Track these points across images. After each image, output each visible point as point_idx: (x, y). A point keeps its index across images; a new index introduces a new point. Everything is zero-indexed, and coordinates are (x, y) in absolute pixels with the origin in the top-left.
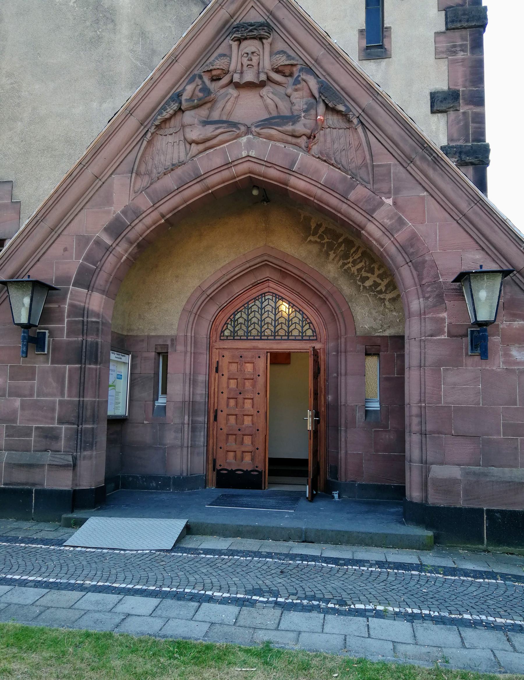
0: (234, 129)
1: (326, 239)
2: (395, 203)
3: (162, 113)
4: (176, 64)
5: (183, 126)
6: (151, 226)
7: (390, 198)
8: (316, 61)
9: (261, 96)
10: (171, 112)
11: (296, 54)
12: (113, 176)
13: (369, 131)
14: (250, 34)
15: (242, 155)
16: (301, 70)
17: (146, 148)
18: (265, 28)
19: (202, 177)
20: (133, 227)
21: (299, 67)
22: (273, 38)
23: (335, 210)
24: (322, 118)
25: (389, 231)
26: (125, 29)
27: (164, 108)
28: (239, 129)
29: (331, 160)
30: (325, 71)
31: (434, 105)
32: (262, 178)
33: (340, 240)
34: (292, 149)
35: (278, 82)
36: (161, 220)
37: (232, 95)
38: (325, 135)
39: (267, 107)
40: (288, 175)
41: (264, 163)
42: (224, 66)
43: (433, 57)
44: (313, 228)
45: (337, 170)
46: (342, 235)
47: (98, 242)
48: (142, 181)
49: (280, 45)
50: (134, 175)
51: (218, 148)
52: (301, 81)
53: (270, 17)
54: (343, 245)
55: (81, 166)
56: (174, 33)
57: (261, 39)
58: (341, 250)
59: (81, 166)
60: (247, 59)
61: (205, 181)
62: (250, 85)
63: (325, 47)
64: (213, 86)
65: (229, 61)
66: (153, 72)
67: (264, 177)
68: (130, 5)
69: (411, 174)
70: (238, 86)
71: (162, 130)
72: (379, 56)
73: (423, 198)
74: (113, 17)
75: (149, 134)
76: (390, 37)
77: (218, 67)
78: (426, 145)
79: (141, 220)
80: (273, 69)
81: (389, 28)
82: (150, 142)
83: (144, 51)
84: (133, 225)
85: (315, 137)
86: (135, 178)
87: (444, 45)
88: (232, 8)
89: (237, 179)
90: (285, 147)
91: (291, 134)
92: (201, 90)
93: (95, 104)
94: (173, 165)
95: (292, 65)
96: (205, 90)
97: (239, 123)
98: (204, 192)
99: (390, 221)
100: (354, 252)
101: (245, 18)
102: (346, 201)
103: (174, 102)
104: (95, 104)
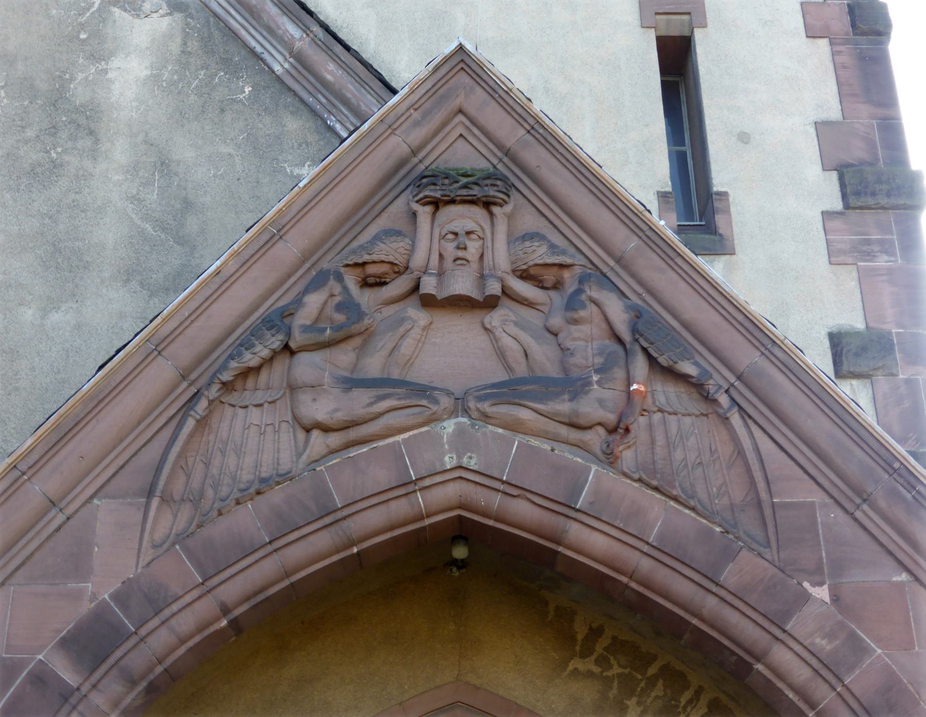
0: (424, 402)
1: (616, 666)
2: (836, 598)
3: (240, 355)
4: (280, 244)
5: (293, 388)
6: (191, 636)
7: (821, 584)
8: (618, 261)
9: (486, 329)
10: (265, 353)
11: (566, 243)
12: (96, 501)
13: (756, 422)
14: (464, 192)
15: (443, 464)
16: (582, 280)
17: (191, 435)
18: (499, 183)
19: (339, 515)
20: (142, 640)
21: (578, 270)
22: (515, 206)
23: (687, 610)
24: (643, 389)
25: (829, 669)
26: (119, 152)
27: (245, 344)
28: (436, 402)
29: (674, 487)
30: (641, 283)
31: (841, 362)
32: (491, 523)
33: (652, 670)
34: (570, 457)
35: (526, 300)
36: (218, 619)
37: (414, 321)
38: (650, 426)
39: (501, 354)
40: (562, 519)
41: (502, 487)
42: (397, 255)
43: (825, 259)
44: (580, 637)
45: (687, 511)
46: (655, 658)
47: (41, 679)
48: (175, 516)
49: (529, 221)
50: (155, 502)
51: (381, 443)
52: (587, 303)
53: (506, 160)
54: (661, 682)
55: (17, 473)
56: (239, 168)
57: (487, 204)
58: (657, 697)
59: (17, 473)
60: (455, 244)
61: (344, 524)
62: (460, 303)
63: (641, 234)
64: (366, 298)
65: (408, 247)
66: (223, 259)
67: (497, 520)
68: (135, 104)
69: (865, 529)
70: (429, 302)
71: (235, 393)
72: (709, 250)
73: (901, 584)
74: (92, 125)
75: (203, 404)
76: (727, 211)
77: (383, 258)
78: (897, 465)
79: (167, 620)
80: (514, 271)
81: (724, 195)
82: (203, 423)
83: (164, 202)
84: (143, 631)
85: (627, 430)
86: (159, 509)
87: (845, 239)
88: (417, 136)
89: (427, 522)
90: (553, 450)
91: (566, 420)
92: (339, 307)
93: (30, 312)
94: (263, 481)
95: (562, 266)
96: (348, 306)
97: (435, 389)
98: (338, 551)
99: (830, 642)
100: (690, 702)
101: (444, 156)
102: (714, 589)
103: (273, 331)
104: (30, 312)
